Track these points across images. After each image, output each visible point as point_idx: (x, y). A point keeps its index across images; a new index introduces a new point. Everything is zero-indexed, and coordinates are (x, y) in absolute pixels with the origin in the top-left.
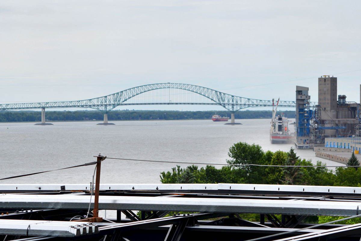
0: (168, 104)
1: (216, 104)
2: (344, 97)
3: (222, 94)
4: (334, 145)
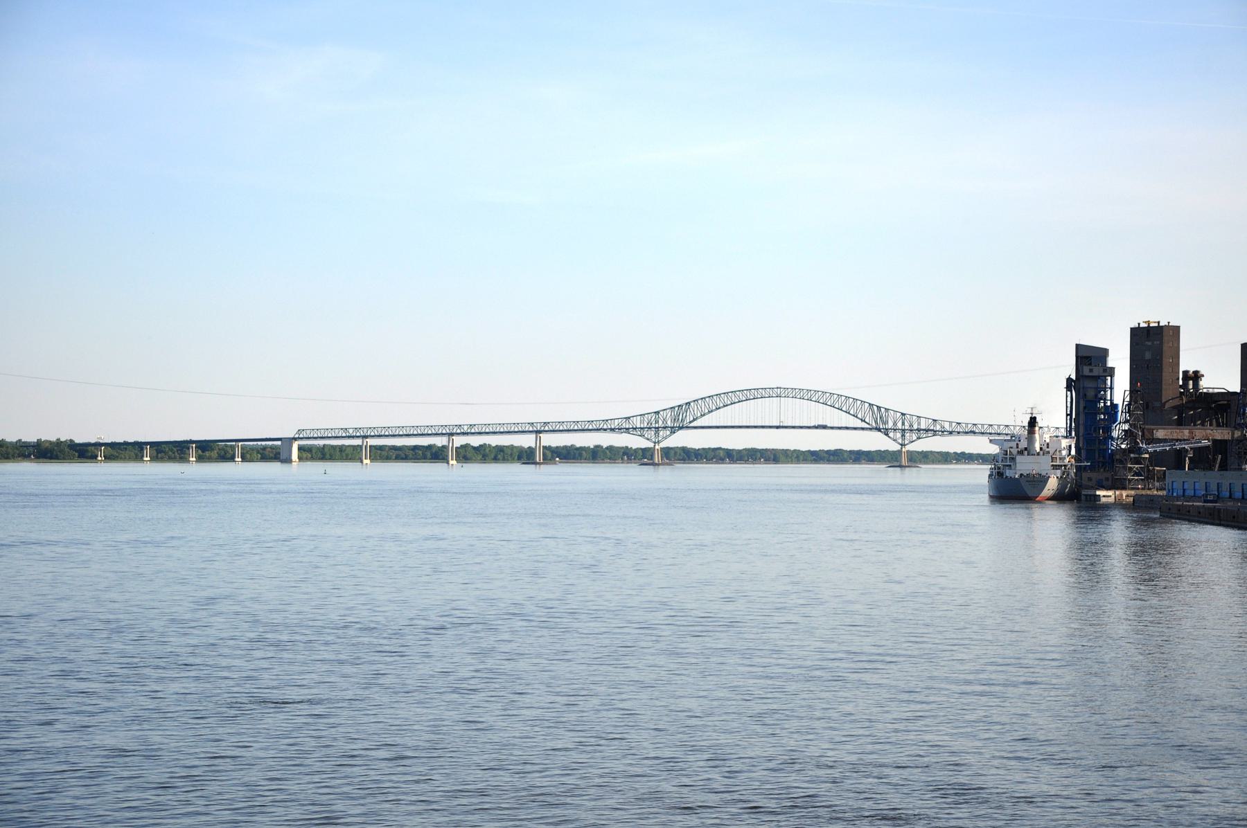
0: (778, 427)
1: (871, 429)
2: (1196, 376)
3: (883, 410)
4: (1195, 490)
